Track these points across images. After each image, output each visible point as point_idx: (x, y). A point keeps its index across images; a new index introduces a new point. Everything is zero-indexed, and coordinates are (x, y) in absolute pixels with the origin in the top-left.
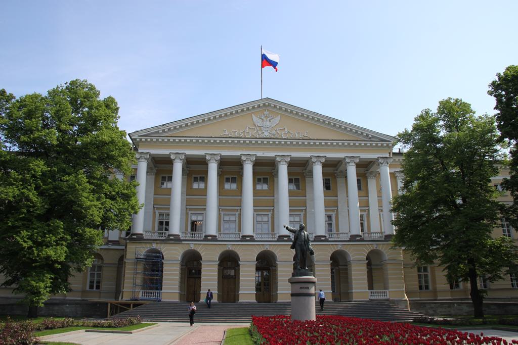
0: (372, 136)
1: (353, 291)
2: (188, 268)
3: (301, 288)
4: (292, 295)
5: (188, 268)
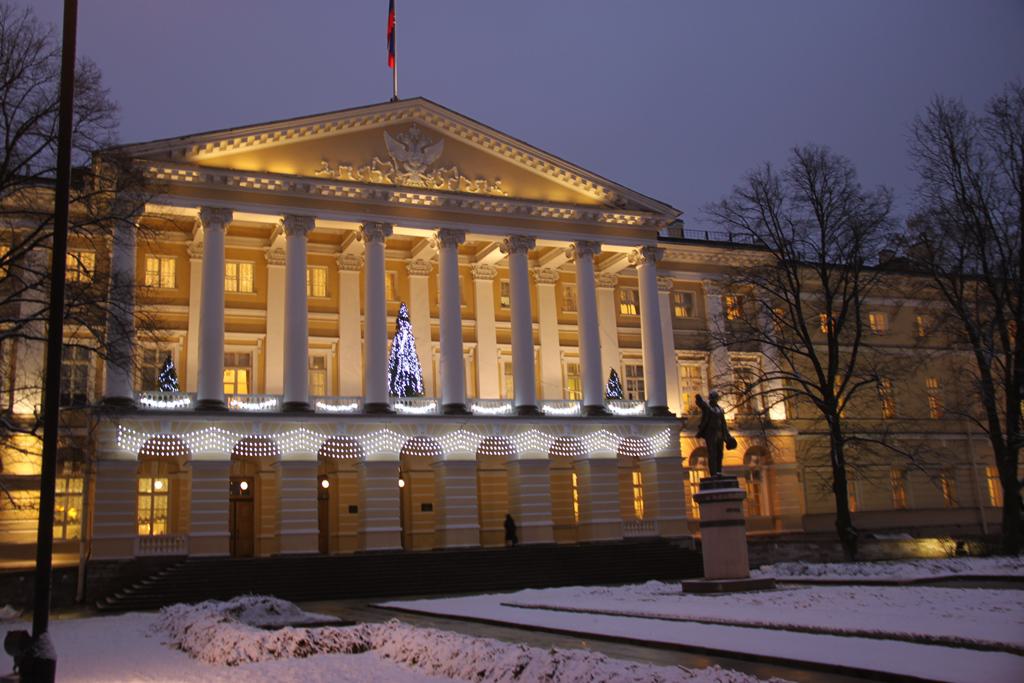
3: (729, 510)
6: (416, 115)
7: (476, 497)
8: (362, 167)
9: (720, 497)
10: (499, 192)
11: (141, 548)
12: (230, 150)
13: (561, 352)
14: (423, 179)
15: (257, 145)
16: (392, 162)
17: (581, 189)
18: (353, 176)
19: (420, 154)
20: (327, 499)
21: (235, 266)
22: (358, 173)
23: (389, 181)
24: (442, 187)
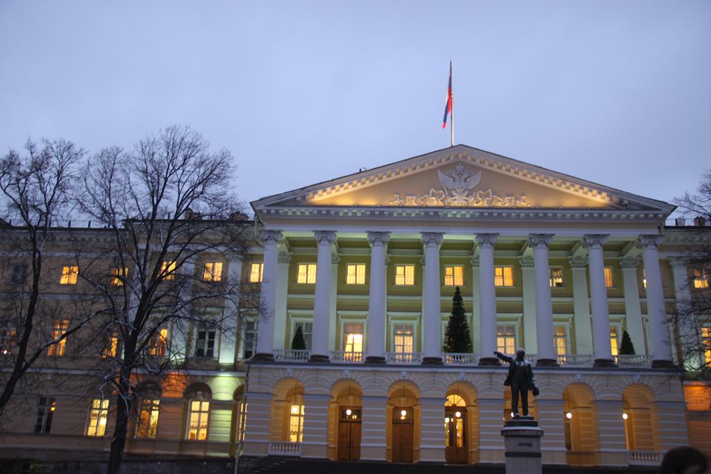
0: (629, 201)
1: (542, 449)
2: (340, 407)
3: (521, 444)
4: (507, 454)
5: (340, 407)
6: (460, 156)
7: (685, 430)
8: (422, 195)
9: (513, 433)
10: (456, 204)
11: (272, 450)
12: (334, 193)
13: (642, 319)
14: (465, 200)
15: (351, 189)
16: (444, 190)
17: (589, 196)
18: (416, 202)
19: (463, 183)
20: (413, 424)
21: (452, 269)
22: (419, 200)
23: (441, 203)
24: (480, 204)
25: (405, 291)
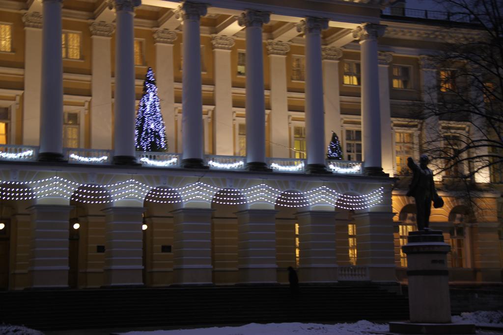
3: (434, 261)
20: (78, 240)
25: (351, 87)
